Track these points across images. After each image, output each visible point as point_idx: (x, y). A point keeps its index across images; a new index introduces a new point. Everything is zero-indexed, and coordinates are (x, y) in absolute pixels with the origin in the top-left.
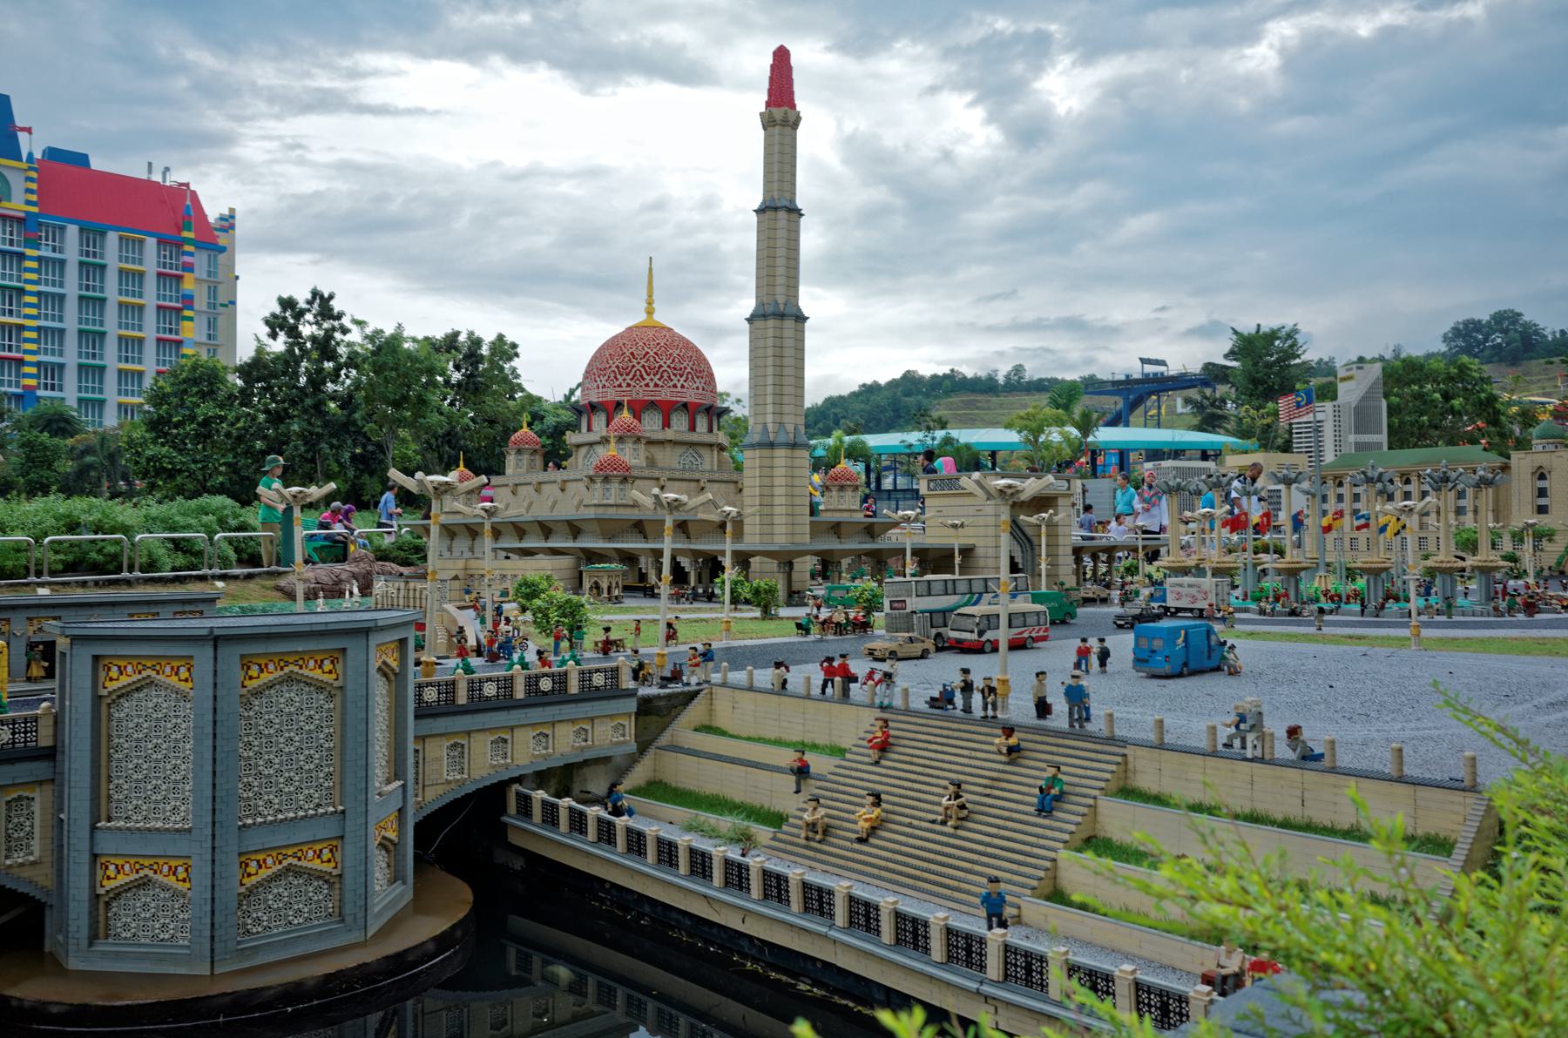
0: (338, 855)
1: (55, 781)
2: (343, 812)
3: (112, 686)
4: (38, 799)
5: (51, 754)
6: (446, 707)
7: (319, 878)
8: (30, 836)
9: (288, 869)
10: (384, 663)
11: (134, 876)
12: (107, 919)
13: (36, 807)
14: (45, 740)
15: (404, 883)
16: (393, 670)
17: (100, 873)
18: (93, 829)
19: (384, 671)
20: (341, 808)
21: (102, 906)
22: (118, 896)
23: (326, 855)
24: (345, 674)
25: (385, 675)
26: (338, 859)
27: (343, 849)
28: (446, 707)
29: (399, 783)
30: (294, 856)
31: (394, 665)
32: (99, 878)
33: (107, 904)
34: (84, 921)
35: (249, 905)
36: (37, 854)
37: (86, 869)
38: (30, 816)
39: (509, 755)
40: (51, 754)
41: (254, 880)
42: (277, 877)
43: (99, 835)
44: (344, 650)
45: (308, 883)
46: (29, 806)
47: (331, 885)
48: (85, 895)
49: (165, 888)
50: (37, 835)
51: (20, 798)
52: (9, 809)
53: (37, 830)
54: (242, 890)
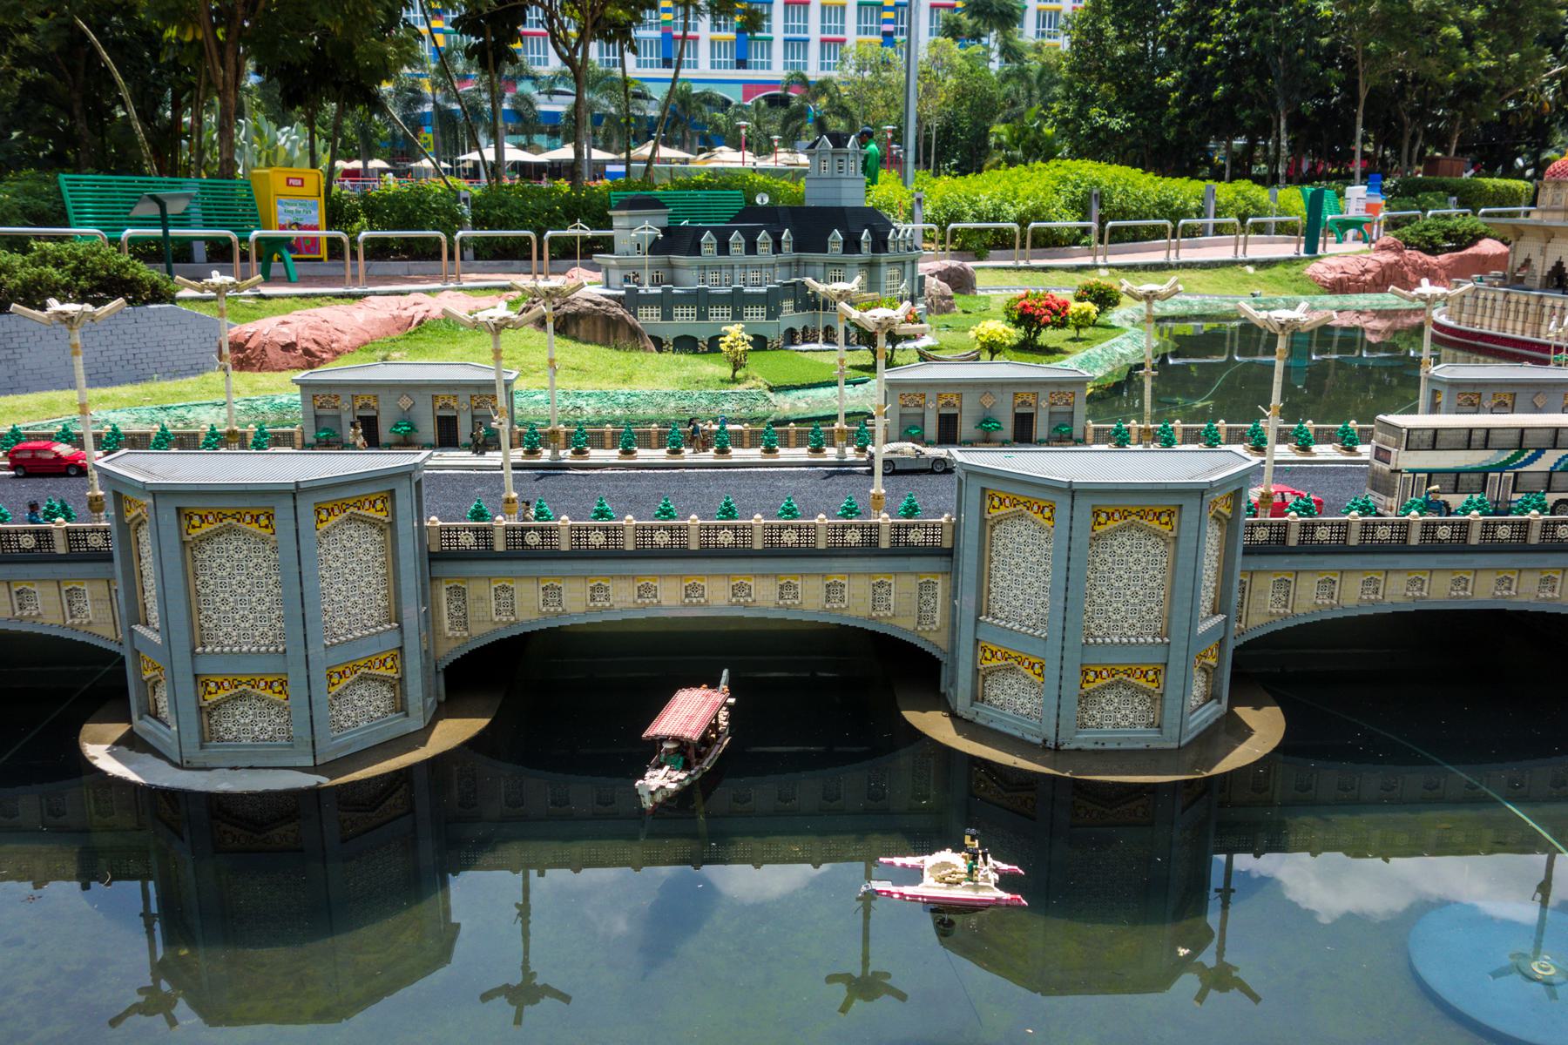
0: (1174, 520)
1: (953, 573)
2: (1168, 644)
3: (995, 512)
4: (940, 585)
5: (949, 553)
6: (1277, 546)
7: (1156, 535)
8: (934, 610)
9: (1119, 682)
10: (1218, 512)
11: (1003, 662)
12: (991, 537)
13: (939, 590)
14: (947, 544)
15: (1219, 702)
16: (1225, 516)
17: (988, 502)
18: (977, 621)
19: (1218, 518)
20: (1166, 640)
21: (980, 678)
22: (999, 522)
23: (1151, 676)
24: (1165, 683)
25: (1218, 520)
26: (1161, 681)
27: (1180, 516)
28: (1277, 546)
29: (1221, 617)
30: (1125, 672)
31: (1227, 512)
32: (987, 506)
33: (992, 528)
34: (968, 686)
35: (1098, 546)
36: (938, 624)
37: (971, 650)
38: (935, 596)
39: (1336, 594)
40: (949, 553)
41: (1092, 686)
42: (1110, 686)
43: (981, 626)
44: (1181, 506)
45: (1147, 537)
46: (934, 588)
47: (1166, 544)
48: (970, 669)
49: (1026, 677)
50: (938, 610)
51: (928, 582)
52: (921, 589)
53: (938, 607)
54: (1082, 692)
